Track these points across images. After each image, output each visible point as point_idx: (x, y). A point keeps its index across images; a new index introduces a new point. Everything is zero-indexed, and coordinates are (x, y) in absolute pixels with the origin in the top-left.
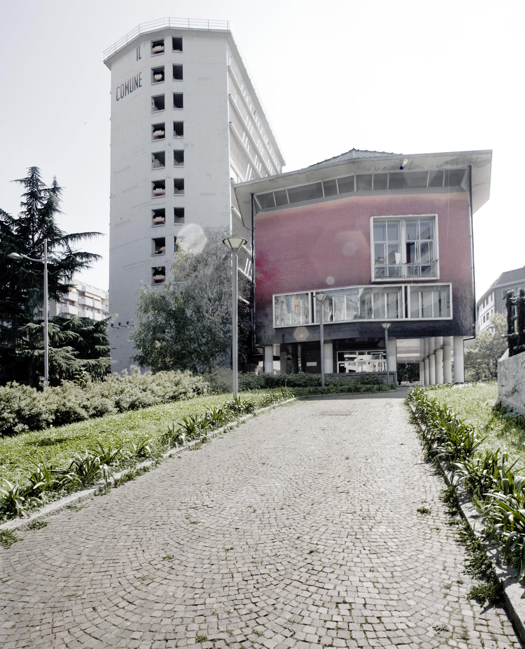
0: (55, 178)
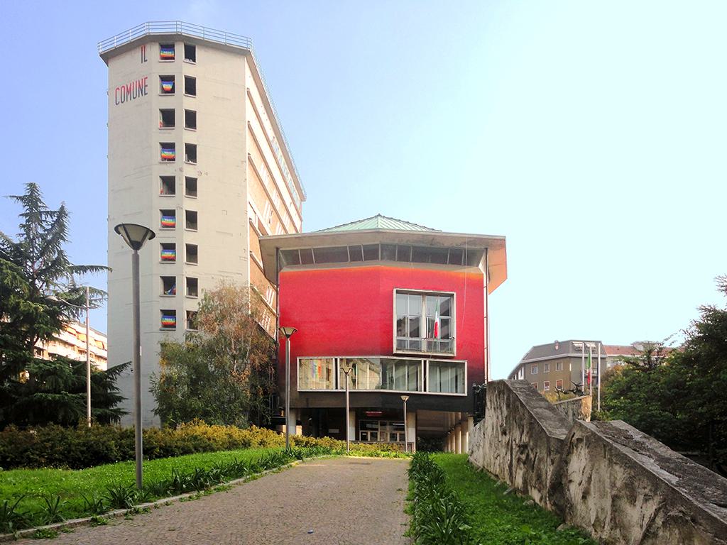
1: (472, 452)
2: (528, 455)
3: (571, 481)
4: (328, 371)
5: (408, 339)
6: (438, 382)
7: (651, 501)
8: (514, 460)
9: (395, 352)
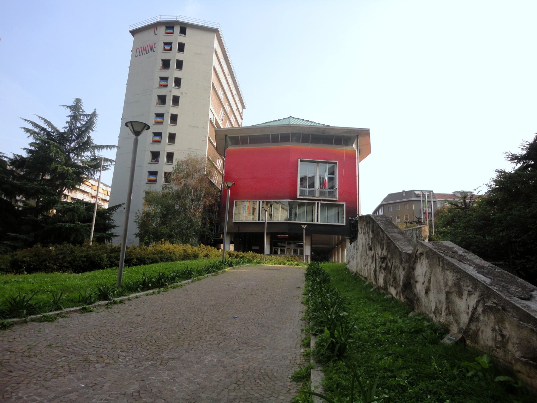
0: (95, 109)
1: (349, 262)
2: (387, 264)
3: (417, 282)
4: (254, 209)
5: (307, 189)
7: (473, 296)
9: (298, 197)
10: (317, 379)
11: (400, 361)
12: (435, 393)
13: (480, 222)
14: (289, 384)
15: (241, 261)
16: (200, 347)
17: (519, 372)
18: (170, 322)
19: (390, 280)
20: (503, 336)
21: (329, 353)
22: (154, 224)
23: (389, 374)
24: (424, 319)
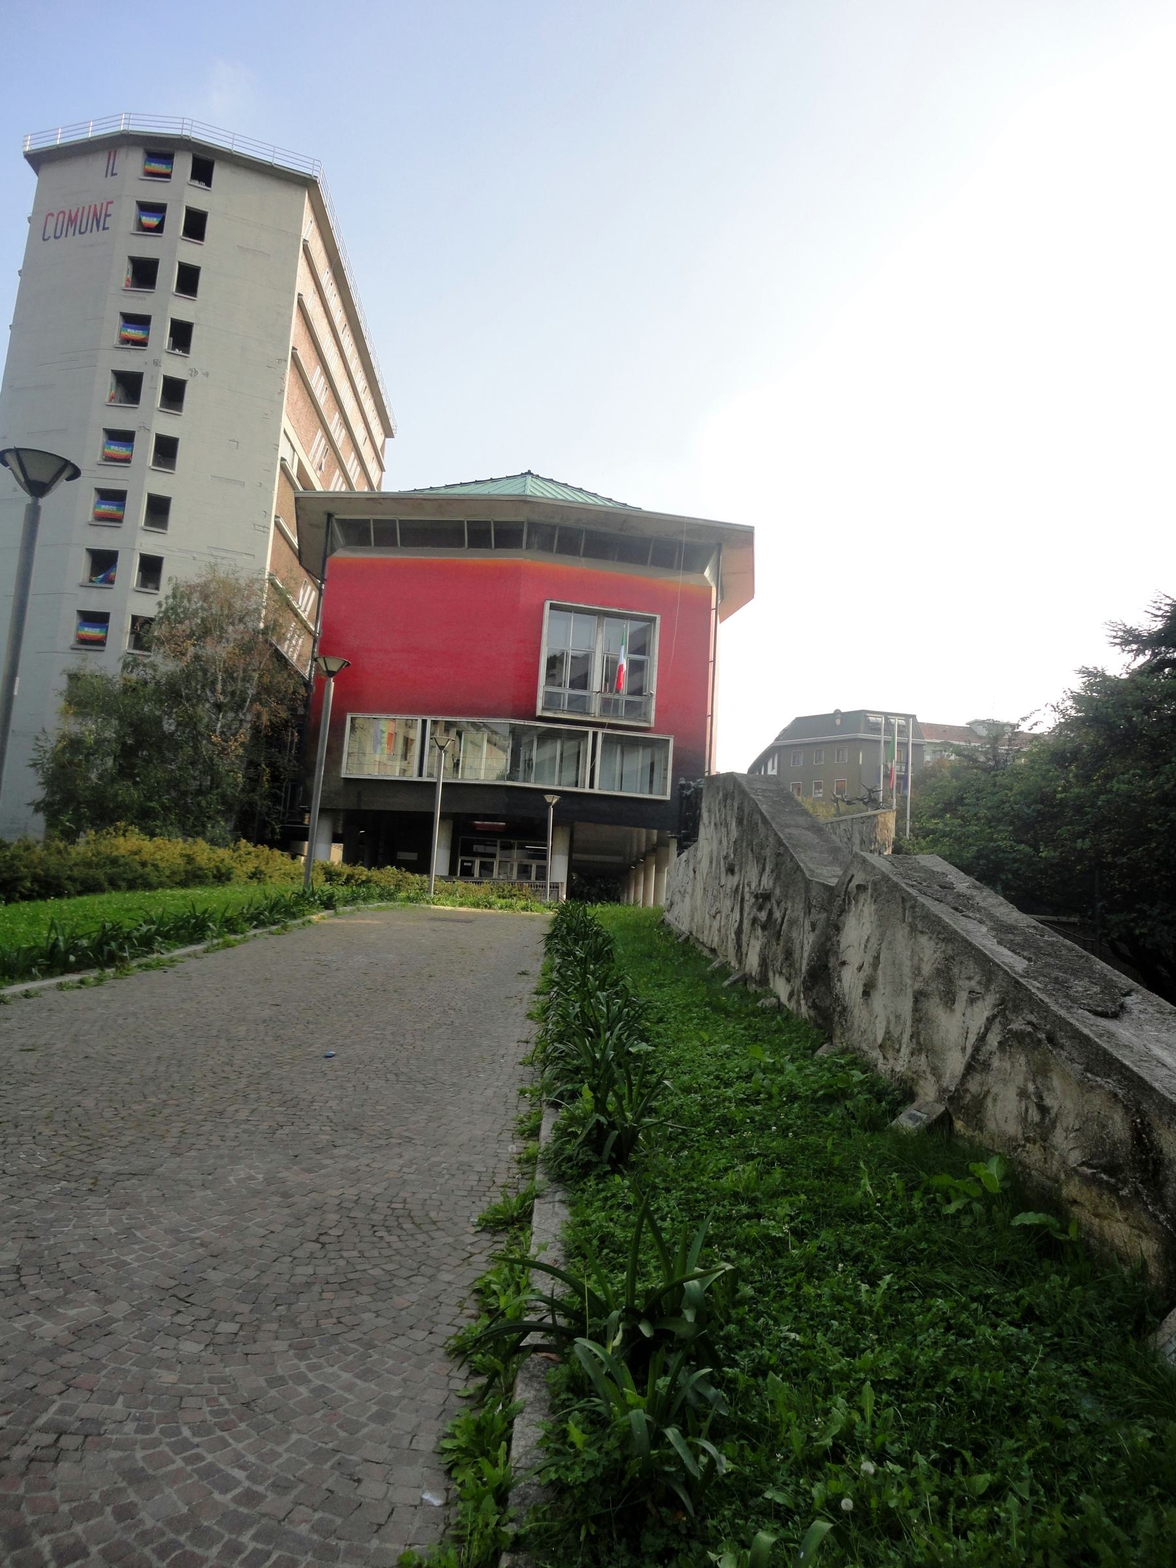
1: (672, 904)
2: (770, 913)
3: (844, 963)
4: (407, 742)
5: (567, 691)
6: (618, 772)
7: (980, 1003)
8: (745, 921)
9: (539, 713)
10: (550, 1226)
11: (778, 1173)
12: (856, 1259)
13: (1029, 807)
14: (470, 1239)
15: (360, 894)
16: (216, 1140)
17: (1075, 1202)
18: (129, 1067)
19: (775, 958)
20: (1043, 1110)
21: (586, 1155)
22: (93, 776)
23: (744, 1208)
24: (853, 1063)
